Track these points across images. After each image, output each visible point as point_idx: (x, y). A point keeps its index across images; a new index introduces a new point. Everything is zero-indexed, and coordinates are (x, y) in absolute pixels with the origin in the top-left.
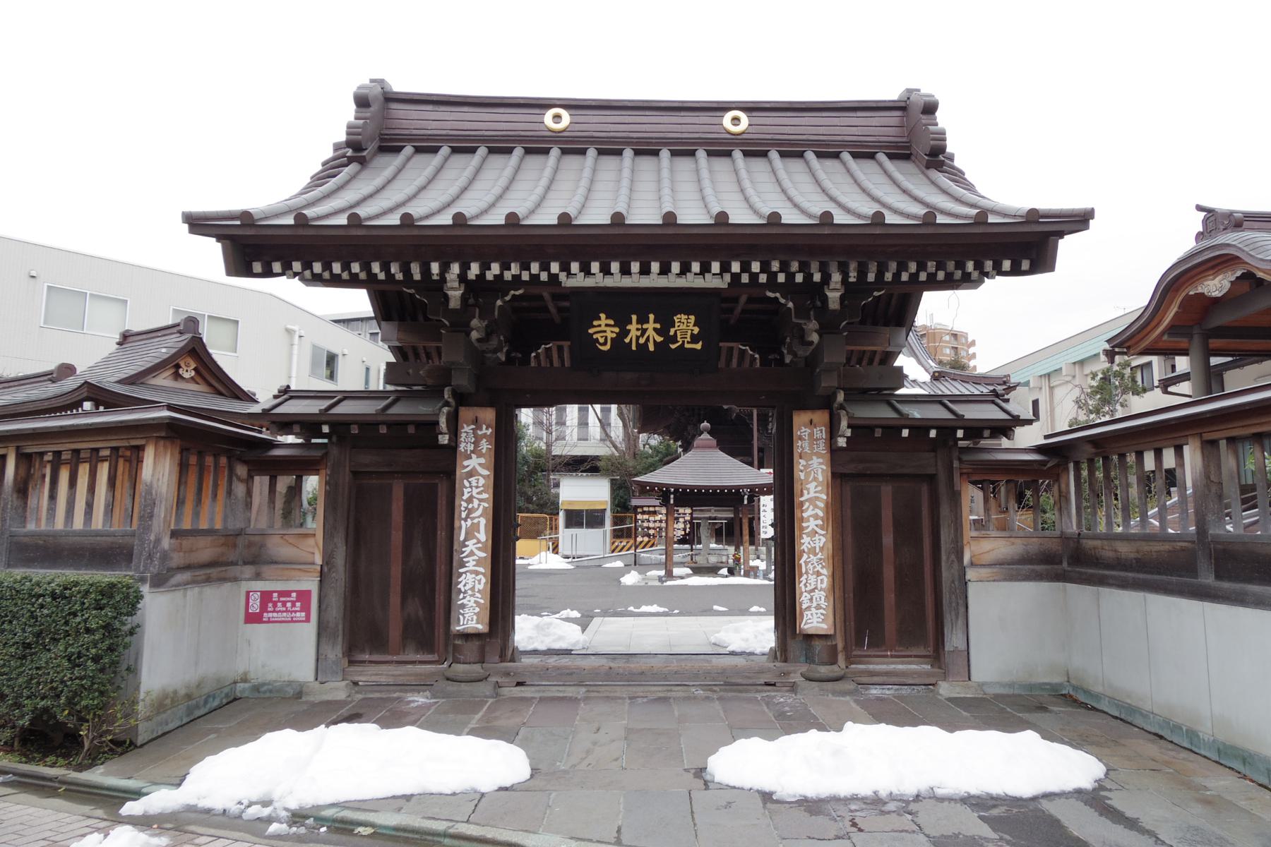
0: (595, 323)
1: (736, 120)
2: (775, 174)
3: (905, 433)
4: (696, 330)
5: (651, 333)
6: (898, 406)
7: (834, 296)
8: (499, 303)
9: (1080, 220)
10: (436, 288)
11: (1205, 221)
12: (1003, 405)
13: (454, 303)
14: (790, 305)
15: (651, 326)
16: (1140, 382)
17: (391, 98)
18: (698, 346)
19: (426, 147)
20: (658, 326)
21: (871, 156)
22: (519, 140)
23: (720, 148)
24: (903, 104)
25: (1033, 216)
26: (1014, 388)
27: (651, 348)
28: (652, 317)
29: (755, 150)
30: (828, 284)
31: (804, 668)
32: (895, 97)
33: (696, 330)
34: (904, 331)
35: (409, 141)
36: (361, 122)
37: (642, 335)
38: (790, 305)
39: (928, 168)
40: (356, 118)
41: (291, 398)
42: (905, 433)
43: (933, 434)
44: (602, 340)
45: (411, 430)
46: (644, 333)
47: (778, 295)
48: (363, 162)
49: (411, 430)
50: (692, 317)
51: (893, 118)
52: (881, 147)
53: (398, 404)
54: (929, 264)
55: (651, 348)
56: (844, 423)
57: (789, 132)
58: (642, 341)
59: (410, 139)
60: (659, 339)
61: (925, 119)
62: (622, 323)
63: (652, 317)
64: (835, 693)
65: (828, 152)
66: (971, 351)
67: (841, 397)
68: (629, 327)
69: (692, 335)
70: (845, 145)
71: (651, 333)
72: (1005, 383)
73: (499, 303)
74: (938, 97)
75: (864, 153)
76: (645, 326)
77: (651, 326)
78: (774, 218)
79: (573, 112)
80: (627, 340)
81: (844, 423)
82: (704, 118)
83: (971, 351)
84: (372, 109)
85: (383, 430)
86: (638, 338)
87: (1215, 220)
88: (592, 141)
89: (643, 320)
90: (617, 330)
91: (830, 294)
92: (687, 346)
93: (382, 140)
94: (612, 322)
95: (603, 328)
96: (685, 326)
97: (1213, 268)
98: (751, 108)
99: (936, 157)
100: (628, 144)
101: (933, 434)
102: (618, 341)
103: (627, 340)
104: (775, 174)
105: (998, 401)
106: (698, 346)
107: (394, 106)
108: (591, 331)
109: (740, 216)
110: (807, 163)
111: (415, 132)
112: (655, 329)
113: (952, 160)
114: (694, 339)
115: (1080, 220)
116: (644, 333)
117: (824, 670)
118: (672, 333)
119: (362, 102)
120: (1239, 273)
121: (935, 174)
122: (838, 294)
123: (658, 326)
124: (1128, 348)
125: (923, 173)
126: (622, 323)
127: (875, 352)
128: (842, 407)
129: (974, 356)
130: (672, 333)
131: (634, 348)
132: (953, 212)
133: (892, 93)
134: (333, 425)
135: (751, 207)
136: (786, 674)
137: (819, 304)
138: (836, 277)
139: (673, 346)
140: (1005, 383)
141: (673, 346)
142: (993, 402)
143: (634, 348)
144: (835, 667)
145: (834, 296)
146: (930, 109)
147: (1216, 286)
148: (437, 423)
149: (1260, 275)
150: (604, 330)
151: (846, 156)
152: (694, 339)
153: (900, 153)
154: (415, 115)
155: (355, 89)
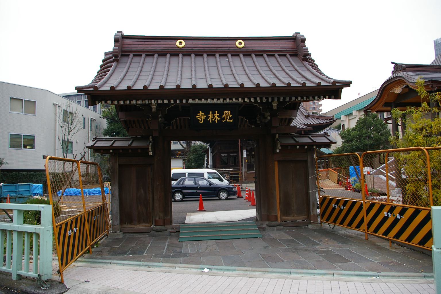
0: (198, 114)
1: (240, 43)
2: (254, 63)
3: (298, 147)
4: (231, 116)
5: (216, 117)
6: (295, 138)
7: (275, 105)
8: (167, 109)
9: (348, 84)
10: (149, 105)
11: (394, 67)
12: (328, 137)
13: (154, 110)
14: (261, 107)
15: (216, 115)
16: (379, 118)
17: (125, 37)
18: (232, 121)
19: (137, 54)
20: (218, 115)
21: (285, 55)
22: (168, 51)
23: (236, 53)
24: (295, 38)
25: (335, 82)
26: (335, 121)
27: (216, 122)
28: (216, 112)
29: (247, 53)
30: (273, 102)
31: (267, 223)
32: (291, 35)
33: (231, 116)
34: (296, 111)
35: (131, 52)
36: (117, 48)
37: (213, 118)
38: (261, 107)
39: (303, 60)
40: (115, 46)
41: (98, 141)
42: (298, 147)
43: (306, 147)
44: (200, 120)
45: (139, 151)
46: (214, 117)
47: (257, 104)
48: (118, 61)
49: (130, 151)
50: (230, 112)
51: (291, 43)
52: (288, 52)
53: (134, 142)
54: (304, 97)
55: (216, 122)
56: (279, 145)
57: (259, 48)
58: (213, 120)
59: (131, 51)
60: (219, 119)
61: (301, 44)
62: (207, 114)
63: (216, 112)
64: (277, 230)
65: (271, 54)
66: (320, 108)
67: (277, 136)
68: (209, 115)
69: (230, 117)
70: (277, 52)
71: (216, 117)
72: (332, 119)
73: (167, 109)
74: (305, 37)
75: (282, 54)
76: (214, 115)
77: (216, 115)
78: (258, 85)
79: (186, 41)
80: (209, 120)
81: (279, 145)
82: (230, 43)
83: (320, 108)
84: (119, 43)
85: (121, 151)
86: (212, 119)
87: (398, 67)
88: (193, 51)
89: (214, 113)
90: (205, 116)
91: (274, 105)
92: (228, 121)
93: (122, 52)
94: (204, 114)
95: (201, 116)
96: (227, 114)
97: (397, 83)
98: (244, 39)
99: (305, 57)
100: (205, 52)
101: (306, 147)
102: (206, 120)
103: (209, 120)
104: (254, 63)
105: (326, 136)
106: (232, 121)
107: (125, 39)
108: (197, 117)
109: (248, 84)
110: (264, 58)
111: (133, 49)
112: (217, 116)
113: (310, 56)
114: (230, 119)
115: (348, 84)
116: (214, 117)
117: (274, 223)
118: (223, 117)
119: (116, 40)
120: (404, 86)
121: (306, 63)
122: (276, 104)
123: (218, 115)
124: (371, 110)
125: (301, 62)
126: (207, 114)
127: (287, 118)
128: (278, 140)
129: (321, 105)
130: (223, 117)
131: (211, 122)
132: (312, 81)
133: (290, 34)
134: (113, 150)
135: (251, 81)
136: (262, 224)
137: (270, 107)
138: (276, 100)
139: (223, 121)
140: (332, 119)
141: (223, 121)
142: (325, 136)
143: (211, 122)
144: (277, 222)
145: (275, 105)
146: (303, 40)
147: (398, 90)
148: (148, 149)
149: (410, 87)
150: (201, 116)
151: (277, 56)
152: (230, 119)
153: (294, 54)
154: (131, 43)
155: (114, 36)
